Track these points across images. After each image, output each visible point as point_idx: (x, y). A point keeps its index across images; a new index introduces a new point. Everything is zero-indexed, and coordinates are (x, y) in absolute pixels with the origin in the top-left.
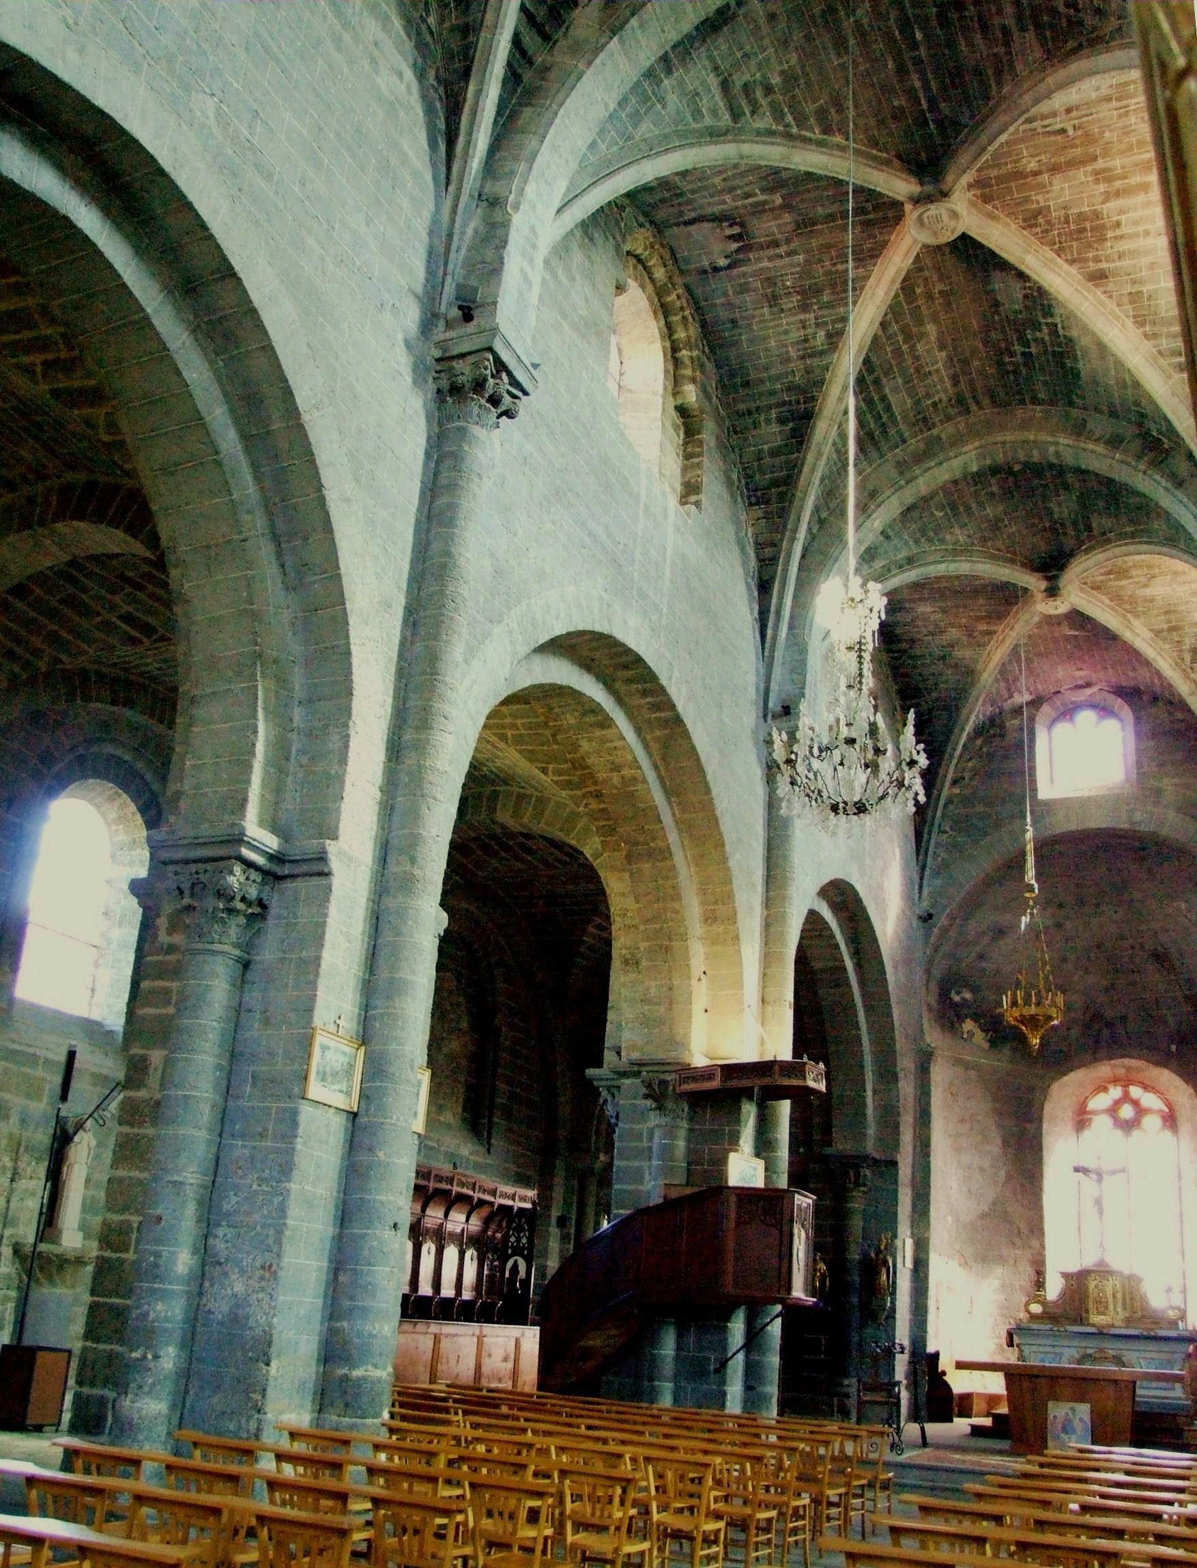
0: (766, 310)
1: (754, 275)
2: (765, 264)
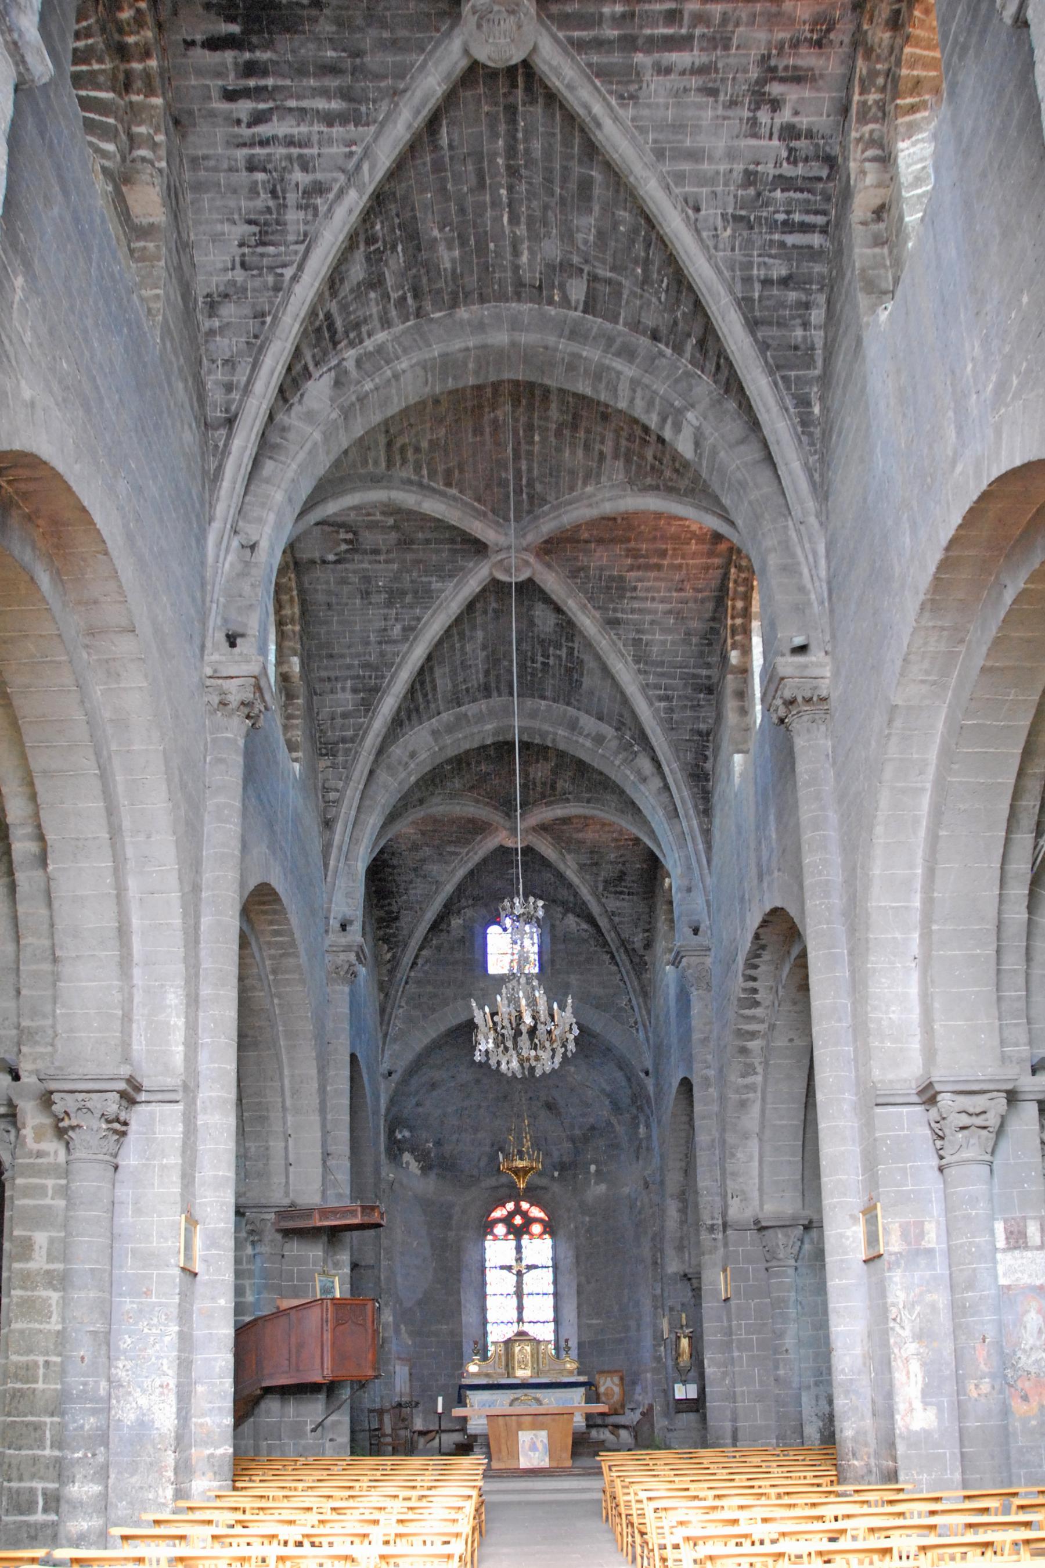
0: (358, 601)
1: (355, 572)
2: (366, 565)
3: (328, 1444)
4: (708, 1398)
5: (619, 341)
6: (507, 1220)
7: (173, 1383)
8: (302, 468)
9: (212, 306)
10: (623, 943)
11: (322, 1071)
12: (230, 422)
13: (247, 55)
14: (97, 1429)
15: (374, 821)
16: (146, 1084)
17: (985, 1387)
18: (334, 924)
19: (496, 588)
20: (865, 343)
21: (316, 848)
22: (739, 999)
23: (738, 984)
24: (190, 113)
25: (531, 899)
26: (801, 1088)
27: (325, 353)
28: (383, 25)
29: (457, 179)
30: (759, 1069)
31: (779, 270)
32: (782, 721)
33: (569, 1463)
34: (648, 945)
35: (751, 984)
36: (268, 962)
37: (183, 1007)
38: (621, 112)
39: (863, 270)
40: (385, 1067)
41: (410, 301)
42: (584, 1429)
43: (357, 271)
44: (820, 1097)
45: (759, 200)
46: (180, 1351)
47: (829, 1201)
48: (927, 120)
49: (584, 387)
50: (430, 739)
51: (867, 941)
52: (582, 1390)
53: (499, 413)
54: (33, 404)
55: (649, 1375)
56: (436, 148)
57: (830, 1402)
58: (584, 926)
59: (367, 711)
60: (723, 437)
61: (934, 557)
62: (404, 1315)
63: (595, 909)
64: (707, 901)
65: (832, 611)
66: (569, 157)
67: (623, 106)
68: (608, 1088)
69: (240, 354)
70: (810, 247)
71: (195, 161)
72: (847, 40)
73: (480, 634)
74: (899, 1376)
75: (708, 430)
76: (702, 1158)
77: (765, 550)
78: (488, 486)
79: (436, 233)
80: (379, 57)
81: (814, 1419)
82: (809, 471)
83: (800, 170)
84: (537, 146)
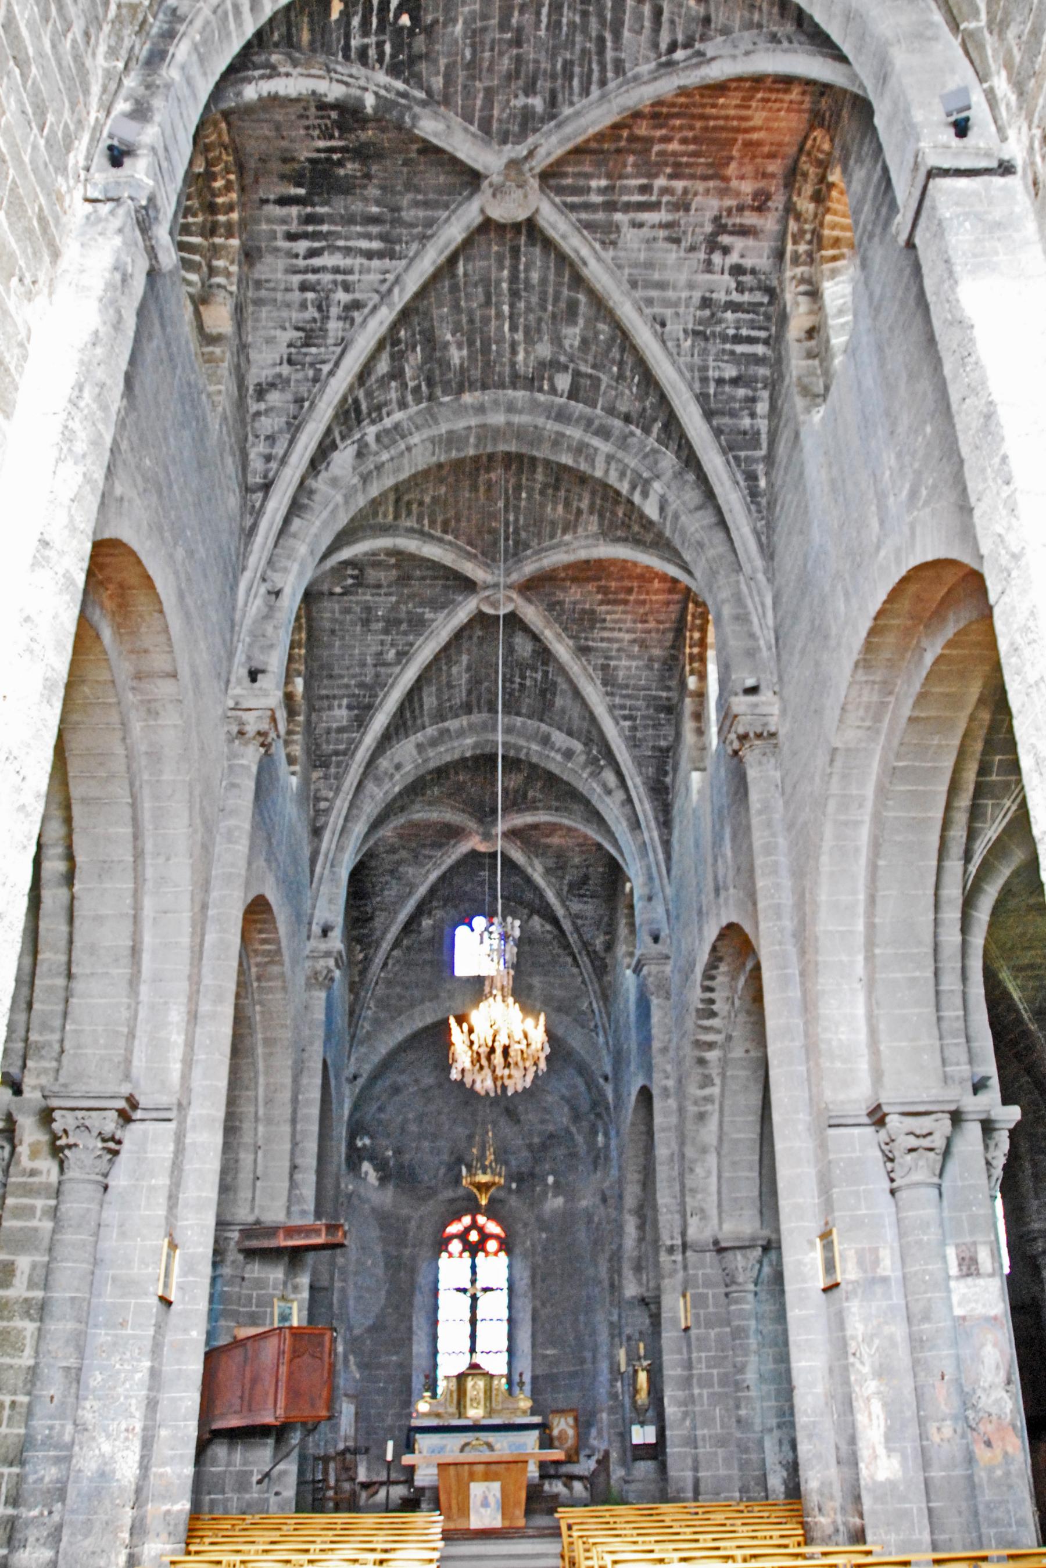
1: (357, 603)
3: (273, 1500)
4: (668, 1443)
5: (597, 423)
6: (463, 1236)
7: (138, 1426)
8: (325, 524)
9: (261, 393)
10: (585, 945)
11: (296, 1079)
12: (267, 487)
13: (309, 210)
14: (58, 1481)
15: (359, 828)
16: (143, 1102)
17: (947, 1431)
18: (316, 929)
19: (480, 619)
20: (802, 436)
21: (306, 852)
22: (698, 1010)
23: (696, 996)
24: (259, 249)
25: (509, 919)
26: (756, 1100)
27: (350, 429)
28: (418, 191)
29: (469, 297)
30: (717, 1081)
31: (730, 371)
32: (736, 753)
33: (521, 1522)
34: (609, 947)
35: (708, 995)
36: (254, 970)
37: (183, 1025)
38: (603, 254)
39: (799, 378)
40: (351, 1070)
41: (424, 388)
42: (537, 1481)
43: (383, 366)
44: (776, 1117)
45: (713, 319)
46: (150, 1389)
47: (786, 1225)
48: (847, 268)
49: (567, 459)
50: (415, 752)
51: (817, 964)
52: (535, 1434)
53: (493, 476)
54: (122, 499)
55: (604, 1415)
56: (454, 276)
57: (794, 1447)
58: (548, 927)
59: (359, 726)
60: (684, 503)
61: (865, 625)
62: (354, 1344)
63: (560, 912)
64: (667, 911)
65: (778, 655)
66: (559, 284)
67: (605, 249)
68: (567, 1094)
69: (281, 431)
70: (755, 355)
71: (258, 284)
72: (781, 207)
73: (465, 658)
74: (861, 1418)
75: (671, 498)
76: (663, 1172)
77: (719, 598)
78: (480, 532)
79: (449, 337)
80: (412, 212)
81: (778, 1467)
82: (757, 534)
83: (746, 297)
84: (535, 276)
